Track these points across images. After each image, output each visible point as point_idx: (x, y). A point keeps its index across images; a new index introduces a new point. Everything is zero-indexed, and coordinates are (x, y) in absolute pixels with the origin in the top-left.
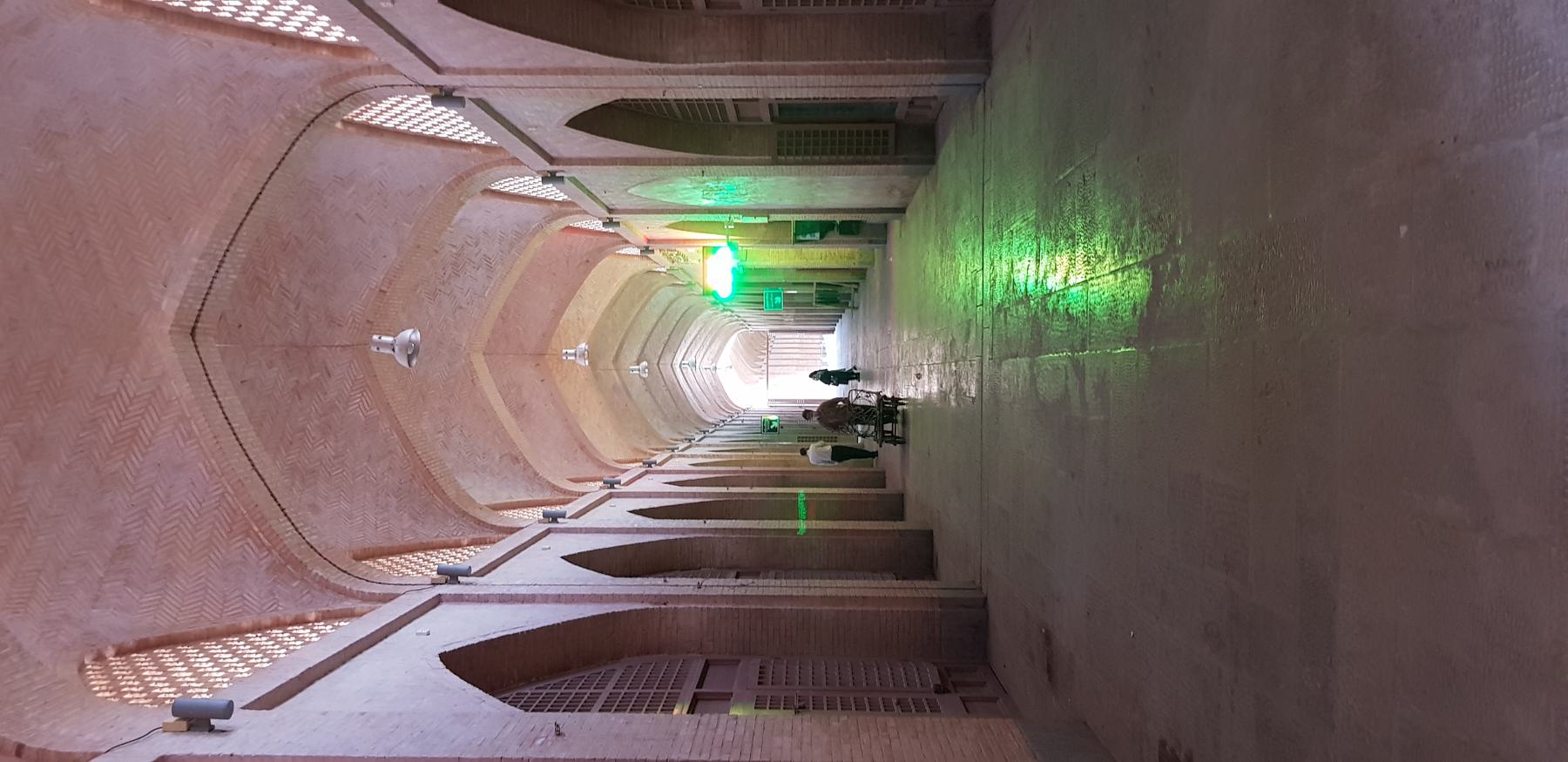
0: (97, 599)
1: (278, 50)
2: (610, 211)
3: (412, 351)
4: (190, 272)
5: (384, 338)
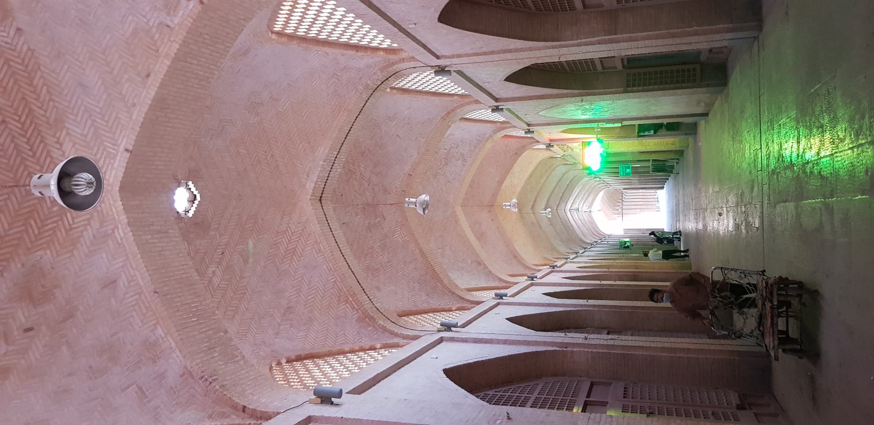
0: (277, 334)
1: (359, 54)
3: (425, 206)
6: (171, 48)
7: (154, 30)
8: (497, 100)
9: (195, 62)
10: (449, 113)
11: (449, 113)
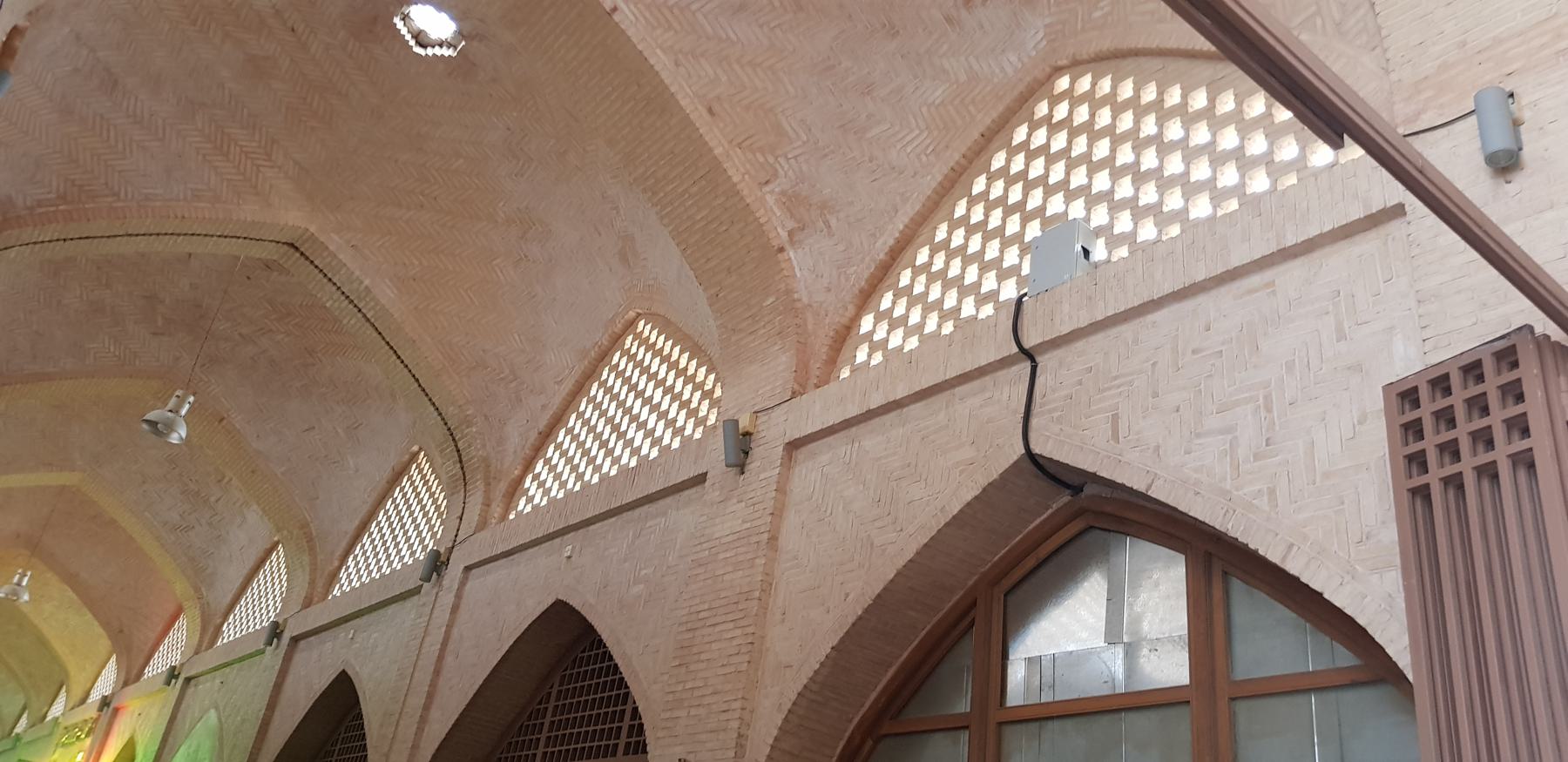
0: (78, 38)
1: (533, 435)
2: (188, 680)
3: (158, 429)
4: (357, 273)
5: (187, 406)
6: (737, 169)
7: (771, 160)
8: (295, 640)
9: (695, 189)
10: (310, 539)
11: (310, 539)
